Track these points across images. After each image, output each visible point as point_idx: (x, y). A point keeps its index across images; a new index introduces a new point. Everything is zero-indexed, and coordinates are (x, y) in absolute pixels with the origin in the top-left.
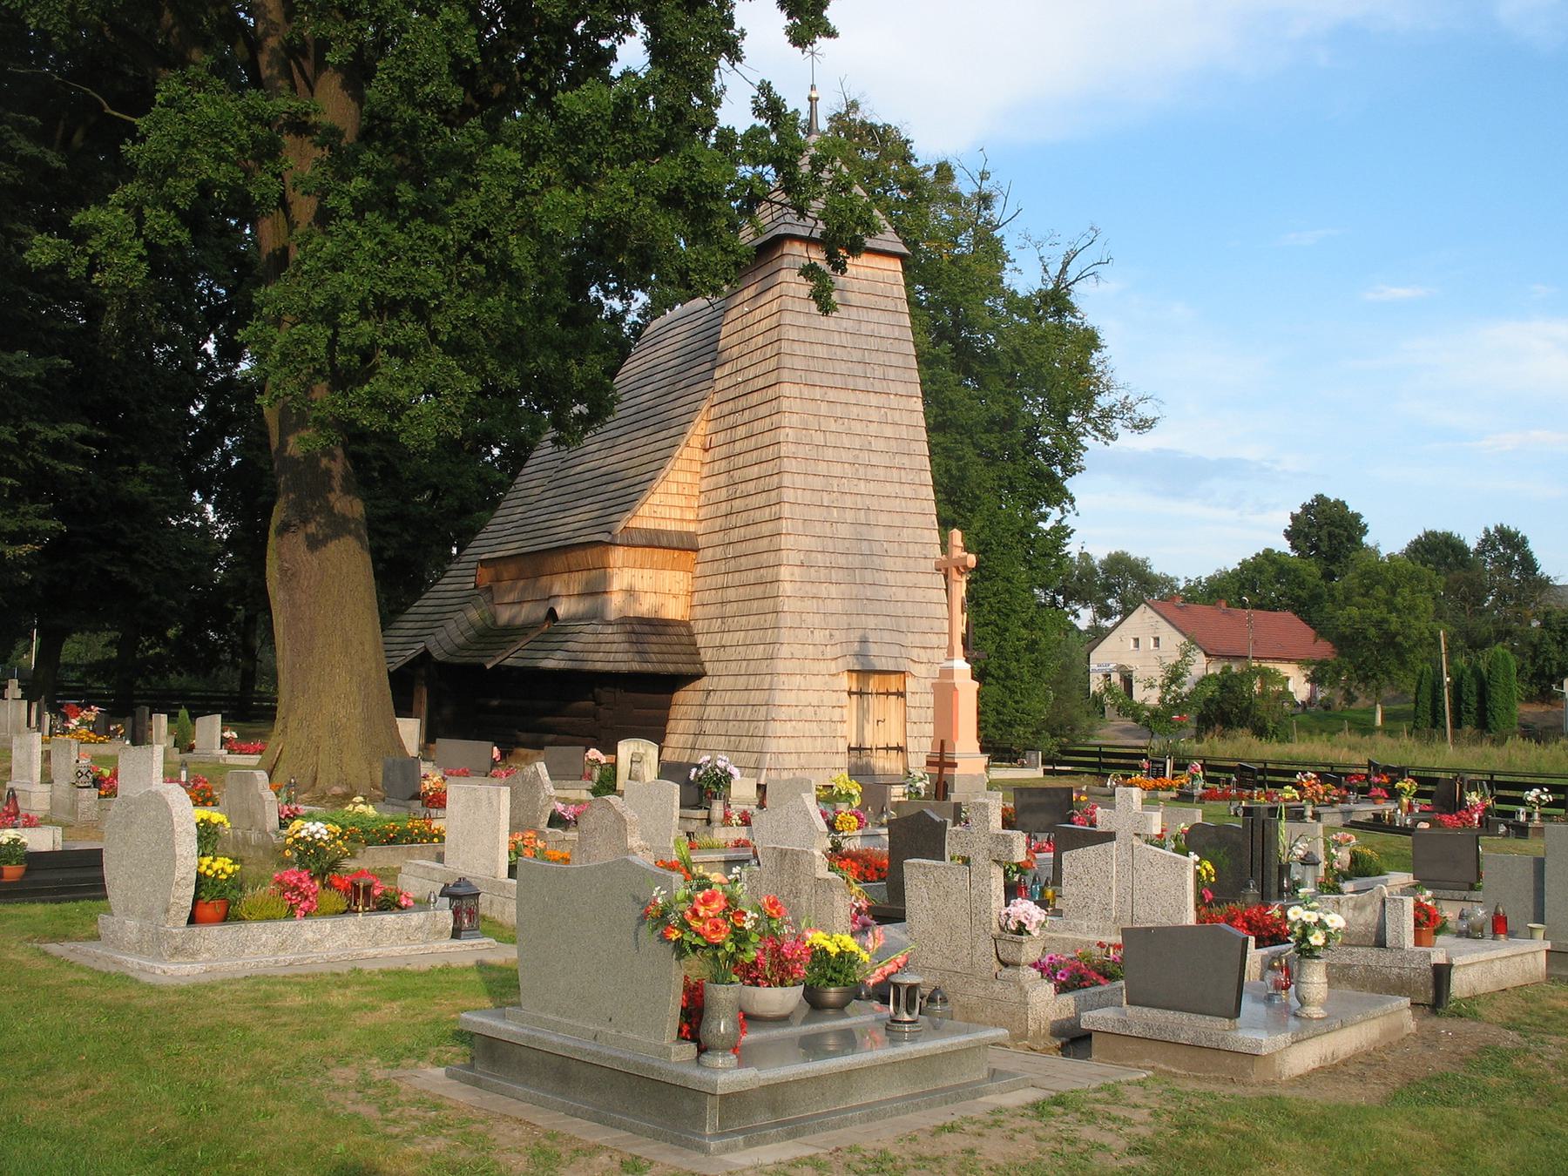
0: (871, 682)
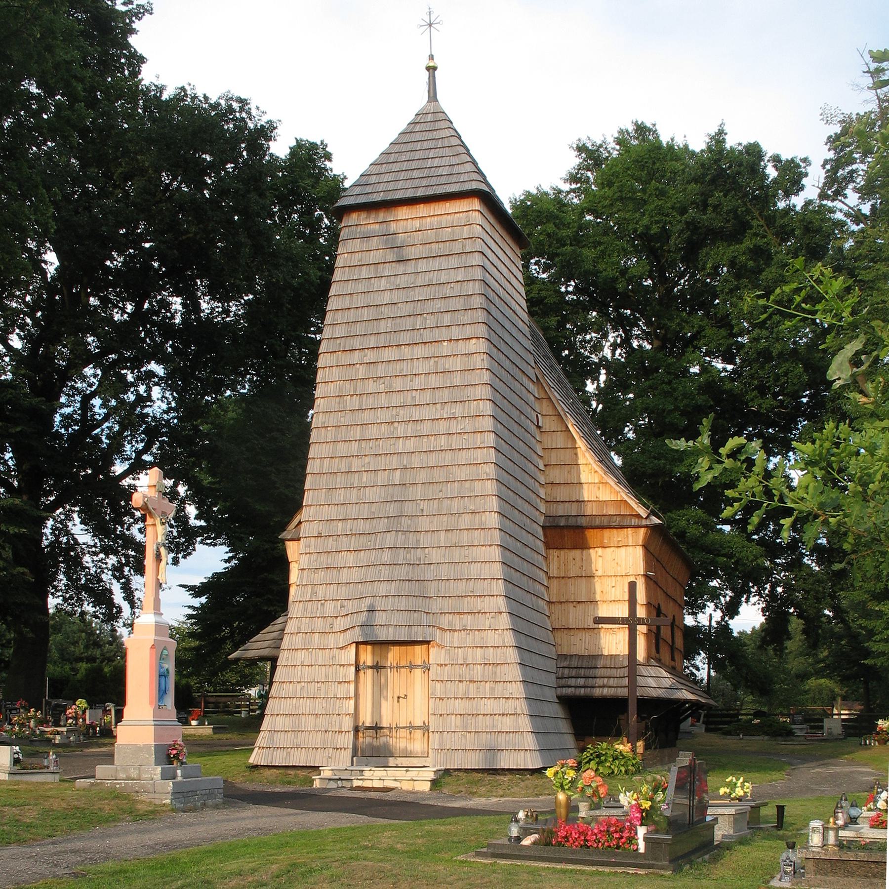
0: (390, 655)
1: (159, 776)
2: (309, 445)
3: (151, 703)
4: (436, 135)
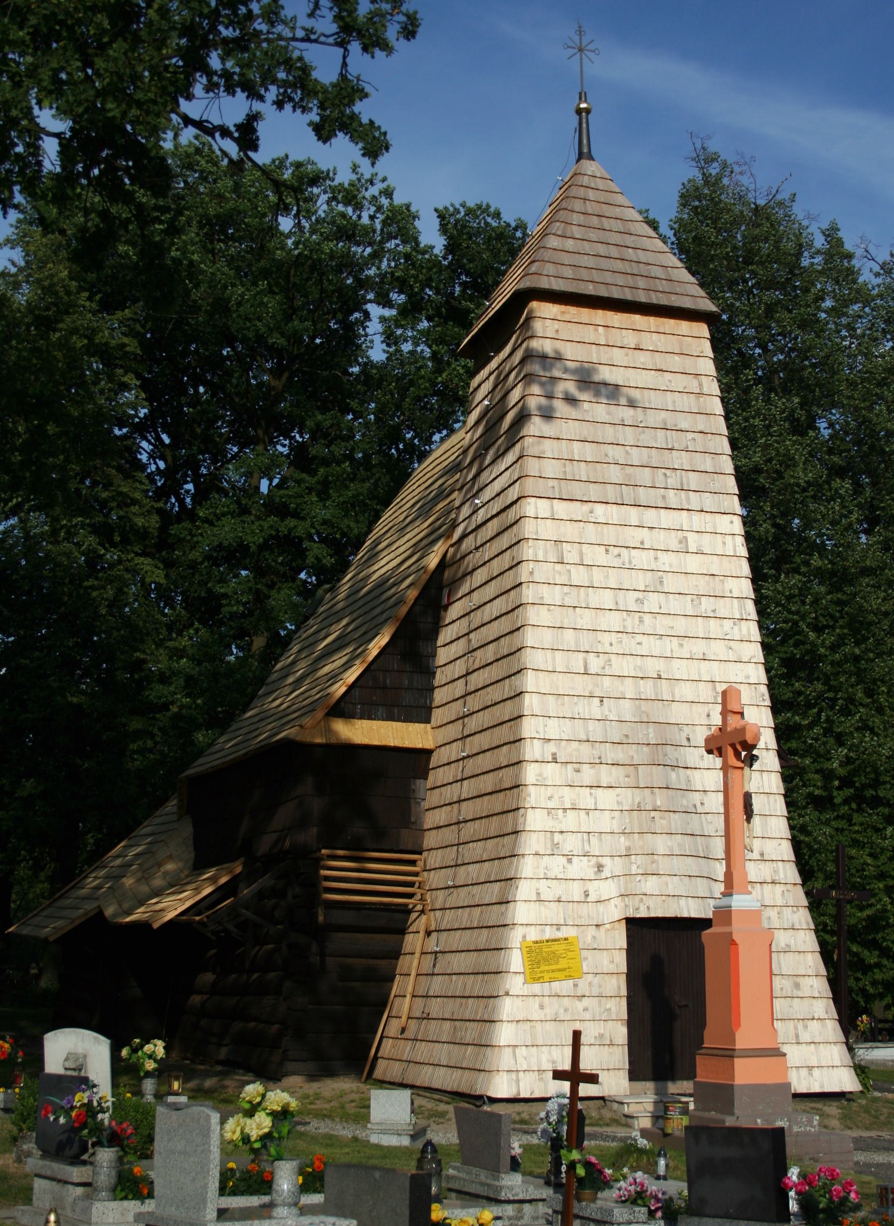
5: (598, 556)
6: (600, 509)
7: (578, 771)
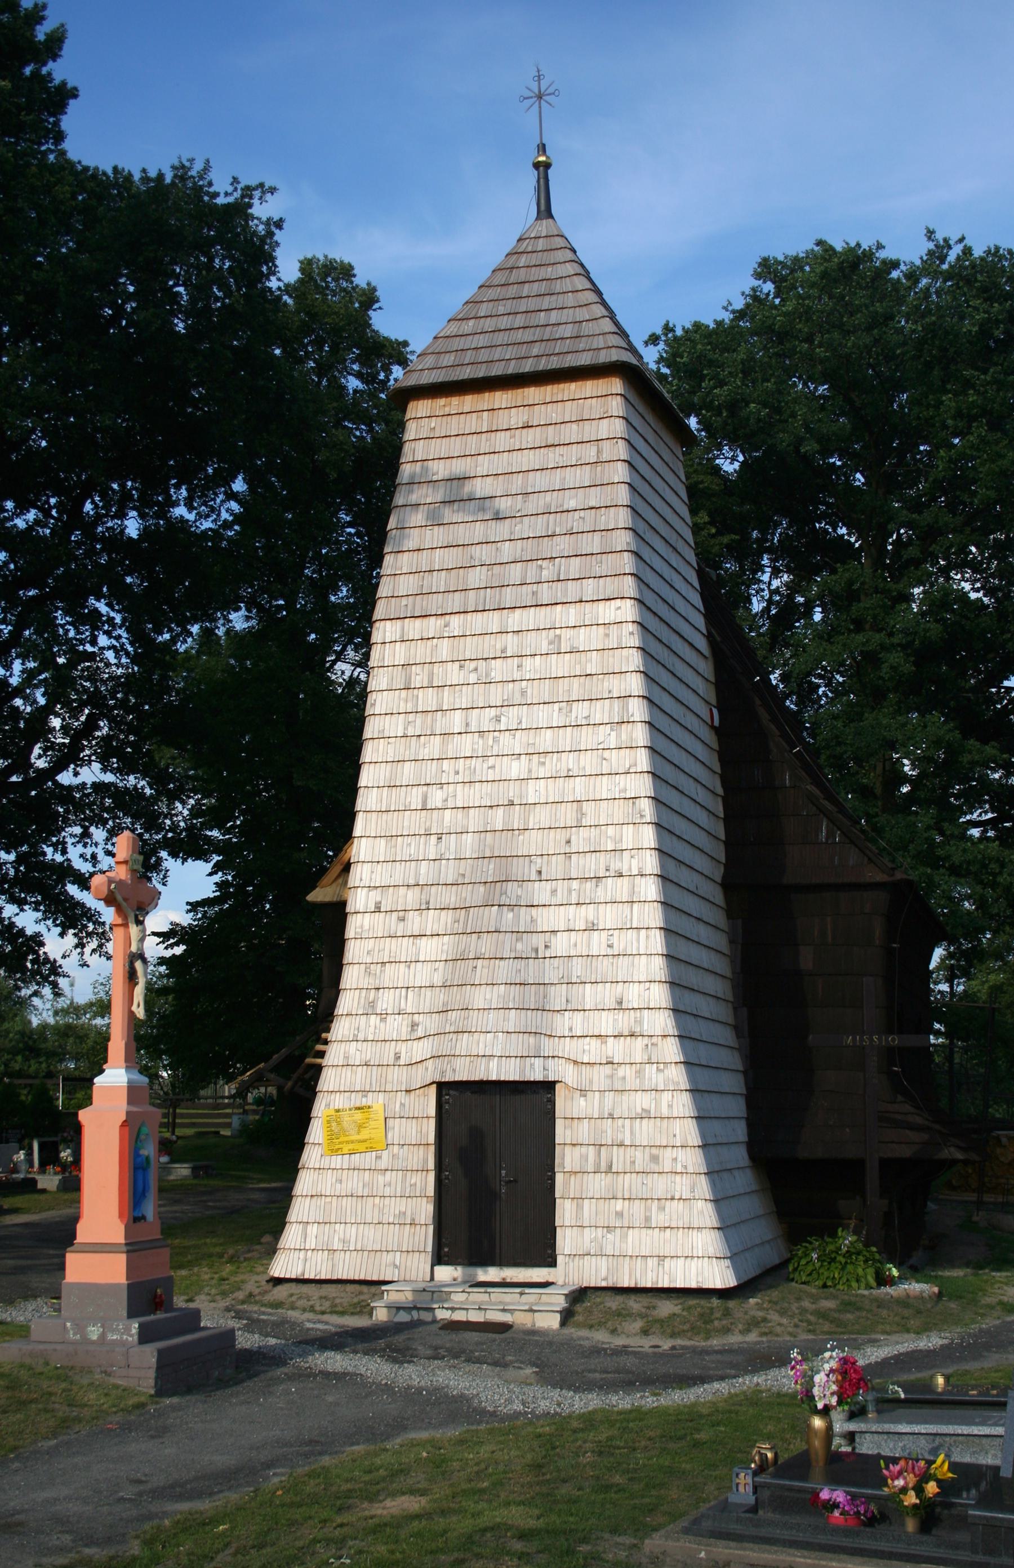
1: (136, 1337)
2: (365, 718)
3: (121, 1216)
4: (549, 272)
5: (454, 674)
6: (455, 621)
7: (402, 919)
